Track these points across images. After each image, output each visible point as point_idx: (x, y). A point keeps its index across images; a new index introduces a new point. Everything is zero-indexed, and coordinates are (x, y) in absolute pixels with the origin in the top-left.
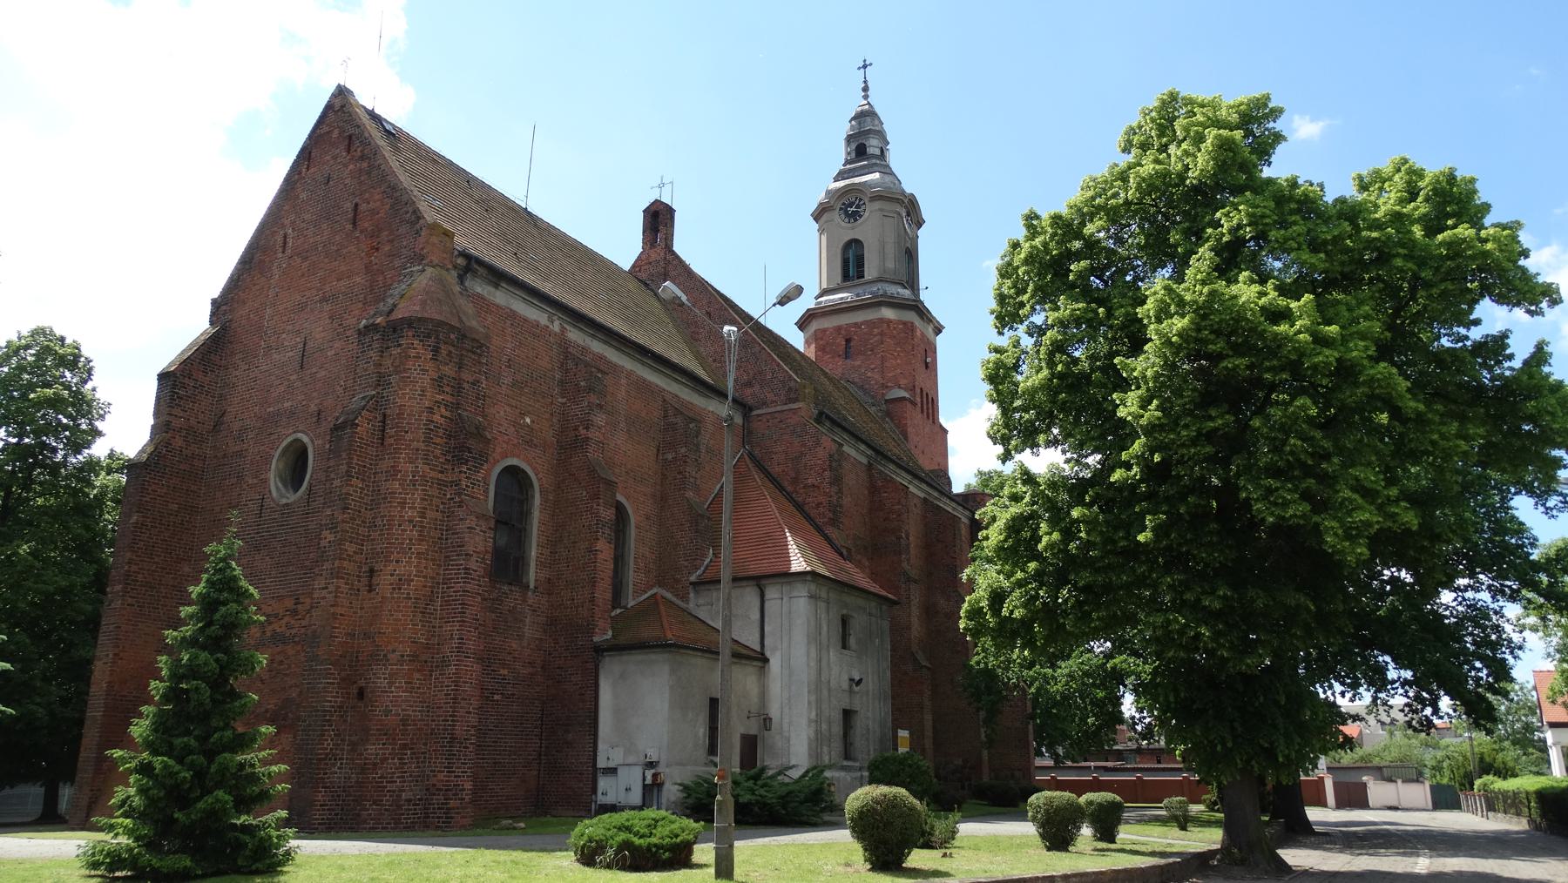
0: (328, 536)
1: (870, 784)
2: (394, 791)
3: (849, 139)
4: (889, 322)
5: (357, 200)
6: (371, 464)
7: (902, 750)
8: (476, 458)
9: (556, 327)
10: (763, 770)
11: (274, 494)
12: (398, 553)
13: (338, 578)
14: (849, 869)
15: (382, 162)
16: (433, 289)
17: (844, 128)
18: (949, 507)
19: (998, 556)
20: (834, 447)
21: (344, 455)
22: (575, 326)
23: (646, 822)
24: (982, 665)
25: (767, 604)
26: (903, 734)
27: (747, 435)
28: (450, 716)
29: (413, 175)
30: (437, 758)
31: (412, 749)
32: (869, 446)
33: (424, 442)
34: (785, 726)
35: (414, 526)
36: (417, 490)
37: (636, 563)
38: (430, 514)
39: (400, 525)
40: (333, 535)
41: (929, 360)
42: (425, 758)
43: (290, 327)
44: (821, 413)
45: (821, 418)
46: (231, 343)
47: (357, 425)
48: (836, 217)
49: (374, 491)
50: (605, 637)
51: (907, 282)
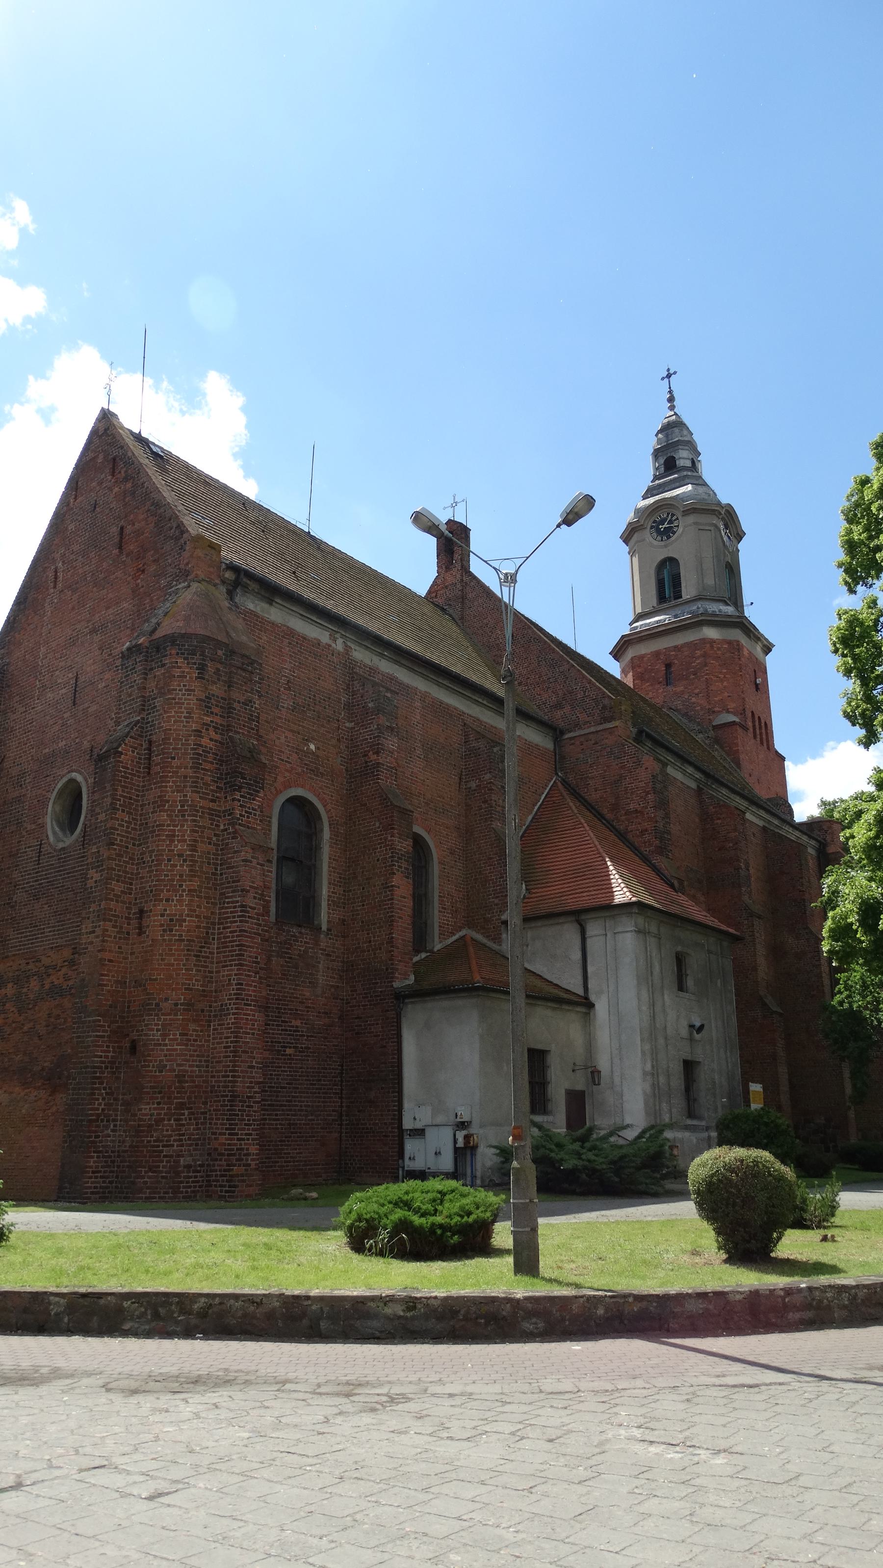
0: (95, 875)
1: (720, 1145)
2: (171, 1156)
3: (657, 454)
4: (712, 642)
5: (122, 523)
6: (138, 796)
7: (755, 1106)
8: (250, 784)
9: (339, 645)
10: (591, 1130)
11: (51, 839)
12: (168, 891)
13: (104, 920)
14: (697, 1259)
15: (145, 479)
16: (198, 603)
17: (651, 443)
18: (794, 835)
19: (869, 857)
20: (657, 767)
21: (108, 785)
22: (361, 645)
23: (430, 1196)
24: (846, 1006)
25: (589, 942)
26: (756, 1088)
27: (559, 760)
28: (231, 1071)
29: (181, 495)
30: (218, 1119)
31: (191, 1108)
32: (698, 768)
33: (191, 768)
34: (617, 1080)
35: (185, 861)
36: (186, 821)
37: (441, 902)
38: (202, 847)
39: (169, 860)
40: (99, 874)
41: (759, 681)
42: (205, 1118)
43: (63, 664)
44: (640, 732)
45: (641, 736)
46: (9, 686)
47: (121, 753)
48: (648, 536)
49: (141, 825)
50: (407, 982)
51: (730, 599)
